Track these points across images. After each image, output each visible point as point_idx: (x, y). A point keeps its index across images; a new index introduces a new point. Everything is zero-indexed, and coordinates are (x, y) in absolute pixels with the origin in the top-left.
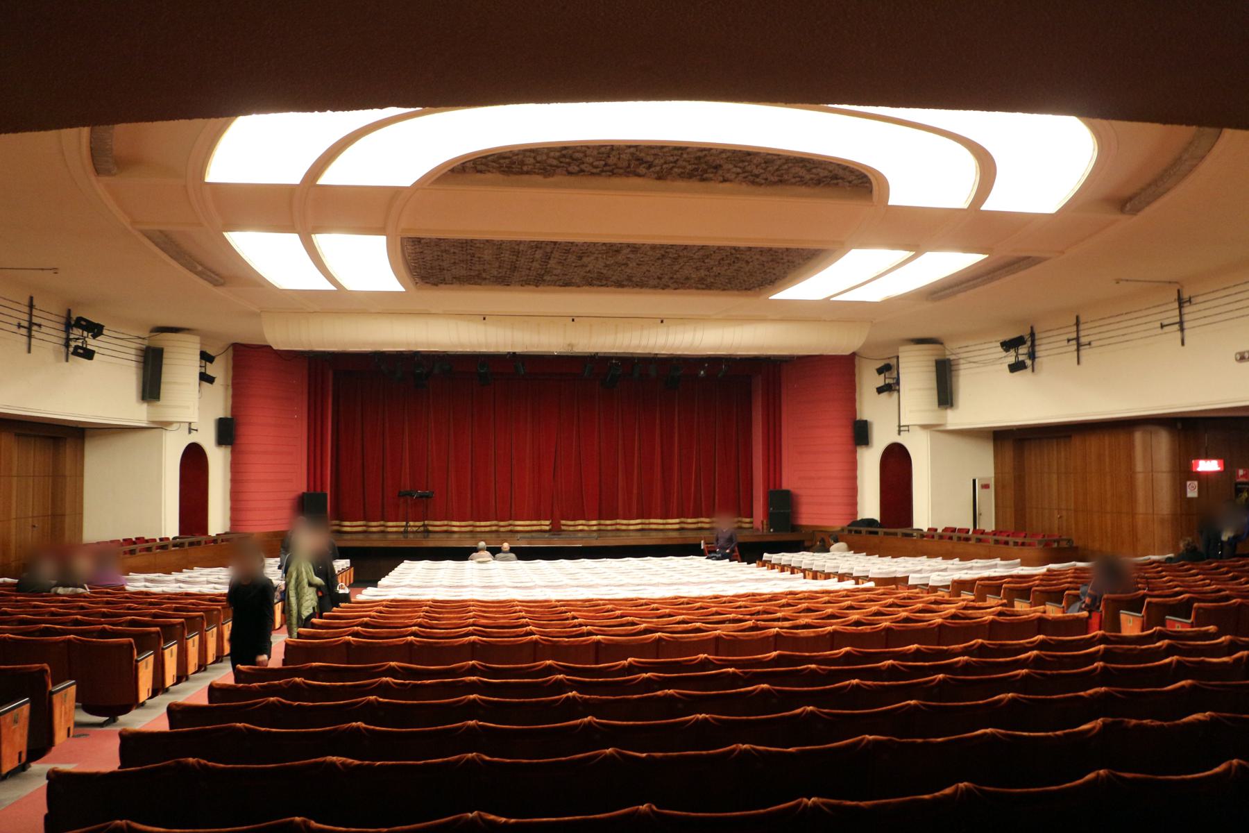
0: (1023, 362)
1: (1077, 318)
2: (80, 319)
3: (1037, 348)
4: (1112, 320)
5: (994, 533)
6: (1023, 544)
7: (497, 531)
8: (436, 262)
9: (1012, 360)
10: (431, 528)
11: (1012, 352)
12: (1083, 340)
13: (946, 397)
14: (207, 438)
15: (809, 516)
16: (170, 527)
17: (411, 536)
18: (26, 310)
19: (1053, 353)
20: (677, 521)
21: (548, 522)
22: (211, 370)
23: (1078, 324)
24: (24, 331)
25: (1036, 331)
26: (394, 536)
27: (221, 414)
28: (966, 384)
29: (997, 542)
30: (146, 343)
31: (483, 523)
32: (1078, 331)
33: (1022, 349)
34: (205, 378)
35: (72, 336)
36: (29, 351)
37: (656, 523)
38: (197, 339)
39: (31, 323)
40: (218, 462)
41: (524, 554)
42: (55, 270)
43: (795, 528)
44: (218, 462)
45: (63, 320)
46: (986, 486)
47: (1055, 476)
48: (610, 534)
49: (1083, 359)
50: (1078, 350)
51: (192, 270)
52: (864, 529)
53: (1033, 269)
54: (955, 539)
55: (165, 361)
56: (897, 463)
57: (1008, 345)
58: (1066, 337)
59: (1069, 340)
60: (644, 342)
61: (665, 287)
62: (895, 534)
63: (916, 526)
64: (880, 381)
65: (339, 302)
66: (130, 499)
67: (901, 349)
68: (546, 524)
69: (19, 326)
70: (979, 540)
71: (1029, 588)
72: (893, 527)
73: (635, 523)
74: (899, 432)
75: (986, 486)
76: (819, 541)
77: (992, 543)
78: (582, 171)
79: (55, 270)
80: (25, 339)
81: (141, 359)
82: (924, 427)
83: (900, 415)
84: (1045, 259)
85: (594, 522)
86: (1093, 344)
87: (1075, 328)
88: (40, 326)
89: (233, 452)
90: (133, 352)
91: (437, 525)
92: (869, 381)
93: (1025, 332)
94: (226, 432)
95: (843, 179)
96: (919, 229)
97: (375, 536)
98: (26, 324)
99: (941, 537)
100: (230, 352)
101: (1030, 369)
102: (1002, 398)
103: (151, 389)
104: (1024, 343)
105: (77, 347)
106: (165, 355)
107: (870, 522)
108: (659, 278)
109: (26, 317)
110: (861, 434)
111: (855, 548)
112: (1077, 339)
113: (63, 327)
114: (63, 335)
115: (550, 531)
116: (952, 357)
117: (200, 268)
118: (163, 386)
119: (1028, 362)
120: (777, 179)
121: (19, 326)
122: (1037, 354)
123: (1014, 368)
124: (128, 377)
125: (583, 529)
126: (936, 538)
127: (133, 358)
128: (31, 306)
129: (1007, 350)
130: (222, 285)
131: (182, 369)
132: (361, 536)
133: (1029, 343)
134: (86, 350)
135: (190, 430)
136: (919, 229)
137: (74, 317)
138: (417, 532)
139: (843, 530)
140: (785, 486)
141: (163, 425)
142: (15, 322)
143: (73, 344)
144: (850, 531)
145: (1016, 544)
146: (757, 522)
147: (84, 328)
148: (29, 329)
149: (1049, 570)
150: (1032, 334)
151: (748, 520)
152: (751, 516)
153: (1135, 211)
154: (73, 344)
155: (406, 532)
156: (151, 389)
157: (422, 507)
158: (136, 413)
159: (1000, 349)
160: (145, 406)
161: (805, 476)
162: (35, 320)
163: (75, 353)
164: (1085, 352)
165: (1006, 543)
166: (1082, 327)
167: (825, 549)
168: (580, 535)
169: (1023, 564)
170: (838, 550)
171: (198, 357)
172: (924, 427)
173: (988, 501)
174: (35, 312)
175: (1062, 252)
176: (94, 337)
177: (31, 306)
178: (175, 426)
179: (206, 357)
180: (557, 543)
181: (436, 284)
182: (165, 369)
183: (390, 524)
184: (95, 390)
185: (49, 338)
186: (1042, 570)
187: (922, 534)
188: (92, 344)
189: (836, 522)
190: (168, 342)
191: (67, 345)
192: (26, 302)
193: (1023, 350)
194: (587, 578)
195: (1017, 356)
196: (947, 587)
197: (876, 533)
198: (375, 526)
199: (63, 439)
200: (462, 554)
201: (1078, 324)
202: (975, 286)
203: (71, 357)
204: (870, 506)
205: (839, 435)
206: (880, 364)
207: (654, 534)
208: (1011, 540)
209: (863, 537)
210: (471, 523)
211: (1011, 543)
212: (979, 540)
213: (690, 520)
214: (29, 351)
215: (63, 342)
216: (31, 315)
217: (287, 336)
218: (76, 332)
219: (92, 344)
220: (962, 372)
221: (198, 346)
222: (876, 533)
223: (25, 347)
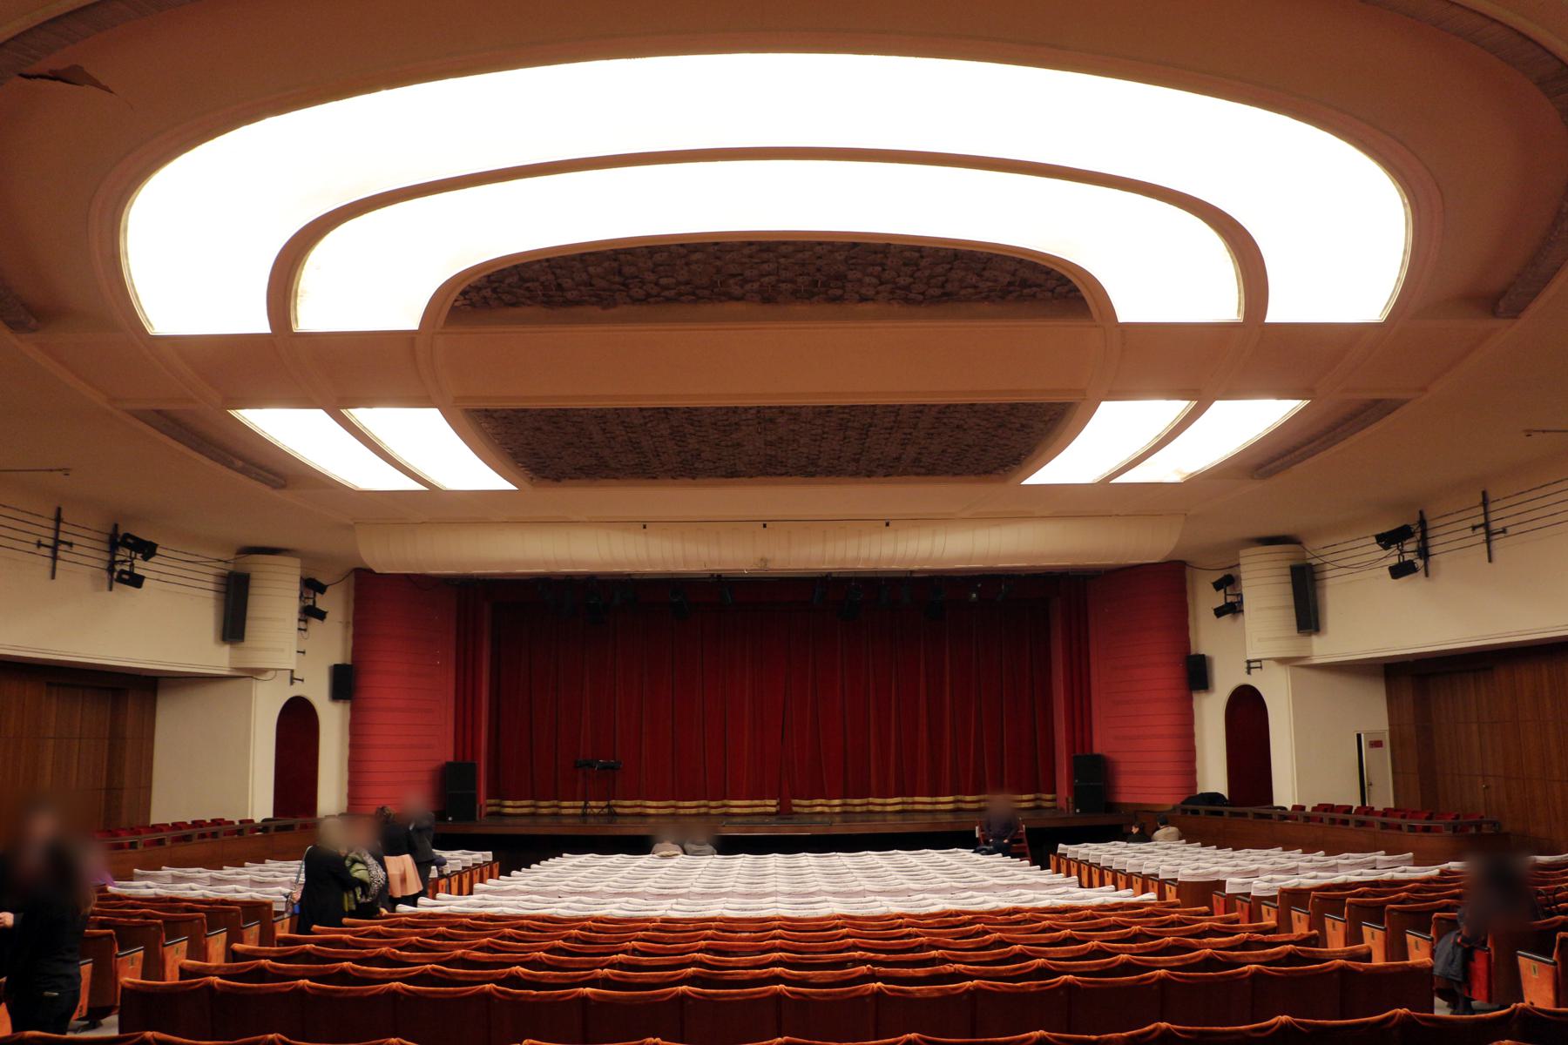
0: (1411, 563)
1: (1484, 494)
2: (127, 535)
3: (1431, 542)
4: (1534, 494)
5: (1386, 812)
6: (1427, 829)
7: (706, 814)
8: (543, 445)
9: (1394, 561)
10: (618, 810)
11: (1394, 549)
12: (1495, 526)
13: (1308, 618)
14: (317, 691)
15: (1132, 790)
16: (261, 806)
17: (591, 820)
18: (52, 524)
19: (1454, 548)
20: (951, 798)
21: (774, 802)
22: (322, 603)
23: (1485, 503)
24: (47, 552)
25: (1428, 516)
26: (571, 821)
27: (338, 661)
28: (1336, 597)
29: (1385, 826)
30: (230, 567)
31: (687, 804)
32: (1486, 514)
33: (1409, 545)
34: (310, 613)
35: (118, 558)
36: (53, 577)
37: (922, 801)
38: (296, 562)
39: (57, 542)
40: (332, 722)
41: (728, 846)
42: (66, 471)
43: (1111, 807)
44: (332, 722)
45: (106, 538)
46: (1377, 744)
47: (1474, 727)
48: (859, 818)
49: (1496, 554)
50: (1488, 542)
51: (230, 465)
52: (1202, 808)
53: (1390, 418)
54: (1326, 821)
55: (252, 591)
56: (1247, 713)
57: (1386, 540)
58: (1469, 523)
59: (1474, 528)
60: (864, 553)
61: (870, 474)
62: (1244, 815)
63: (1276, 803)
64: (1219, 599)
65: (431, 507)
66: (218, 766)
67: (1242, 553)
68: (771, 805)
69: (39, 544)
70: (1362, 824)
71: (1382, 905)
72: (1244, 812)
73: (893, 803)
74: (1249, 669)
75: (1377, 744)
76: (1133, 825)
77: (1377, 827)
78: (648, 295)
79: (66, 471)
80: (48, 561)
81: (222, 588)
82: (1282, 661)
83: (1248, 644)
84: (1402, 403)
85: (836, 802)
86: (1510, 530)
87: (1481, 510)
88: (71, 545)
89: (354, 711)
90: (211, 578)
91: (626, 806)
92: (1205, 599)
93: (1411, 520)
94: (343, 683)
95: (1039, 286)
96: (1193, 363)
97: (546, 820)
98: (50, 542)
99: (1308, 818)
100: (352, 579)
101: (1421, 572)
102: (1386, 617)
103: (233, 627)
104: (1412, 535)
105: (123, 572)
106: (252, 583)
107: (1214, 798)
108: (857, 461)
109: (51, 533)
110: (1198, 674)
111: (1188, 835)
112: (1486, 525)
113: (106, 547)
114: (107, 557)
115: (777, 813)
116: (1314, 562)
117: (240, 464)
118: (249, 623)
119: (1419, 563)
120: (938, 292)
121: (39, 544)
122: (1432, 551)
123: (1399, 571)
124: (204, 612)
125: (825, 809)
126: (1301, 821)
127: (211, 586)
128: (58, 520)
129: (1386, 547)
130: (283, 487)
131: (275, 603)
132: (524, 821)
133: (1418, 536)
134: (131, 573)
135: (292, 680)
136: (1193, 363)
137: (121, 532)
138: (598, 815)
139: (1174, 809)
140: (1097, 749)
141: (255, 673)
142: (34, 539)
143: (118, 568)
144: (1184, 811)
145: (1412, 829)
146: (1060, 799)
147: (128, 546)
148: (55, 549)
149: (1442, 873)
150: (1423, 522)
151: (1049, 797)
152: (1053, 791)
153: (1515, 312)
154: (118, 568)
155: (584, 815)
156: (233, 627)
157: (608, 782)
158: (216, 658)
159: (1378, 547)
160: (227, 648)
161: (1124, 734)
162: (62, 537)
163: (121, 580)
164: (1498, 543)
165: (1399, 827)
166: (1492, 507)
167: (1145, 837)
168: (818, 819)
169: (1417, 862)
170: (1166, 837)
171: (297, 586)
172: (1282, 661)
173: (1381, 767)
174: (63, 527)
175: (1424, 389)
176: (146, 558)
177: (58, 520)
178: (270, 675)
179: (311, 586)
180: (787, 831)
181: (557, 479)
182: (252, 601)
183: (565, 804)
184: (156, 626)
185: (85, 560)
186: (1434, 871)
187: (1283, 814)
188: (141, 567)
189: (1167, 798)
190: (260, 566)
191: (111, 570)
192: (53, 515)
193: (1411, 546)
194: (900, 881)
195: (1402, 553)
196: (1272, 899)
197: (1220, 813)
198: (545, 806)
199: (131, 693)
200: (640, 846)
201: (1485, 503)
202: (1313, 453)
203: (116, 585)
204: (1214, 776)
205: (1163, 677)
206: (1219, 575)
207: (921, 818)
208: (1405, 822)
209: (1205, 821)
210: (672, 802)
211: (1405, 828)
212: (1362, 824)
213: (968, 798)
214: (53, 577)
215: (104, 565)
216: (57, 530)
217: (392, 555)
218: (123, 553)
219: (141, 567)
220: (1329, 582)
221: (298, 572)
222: (1220, 813)
223: (48, 572)
